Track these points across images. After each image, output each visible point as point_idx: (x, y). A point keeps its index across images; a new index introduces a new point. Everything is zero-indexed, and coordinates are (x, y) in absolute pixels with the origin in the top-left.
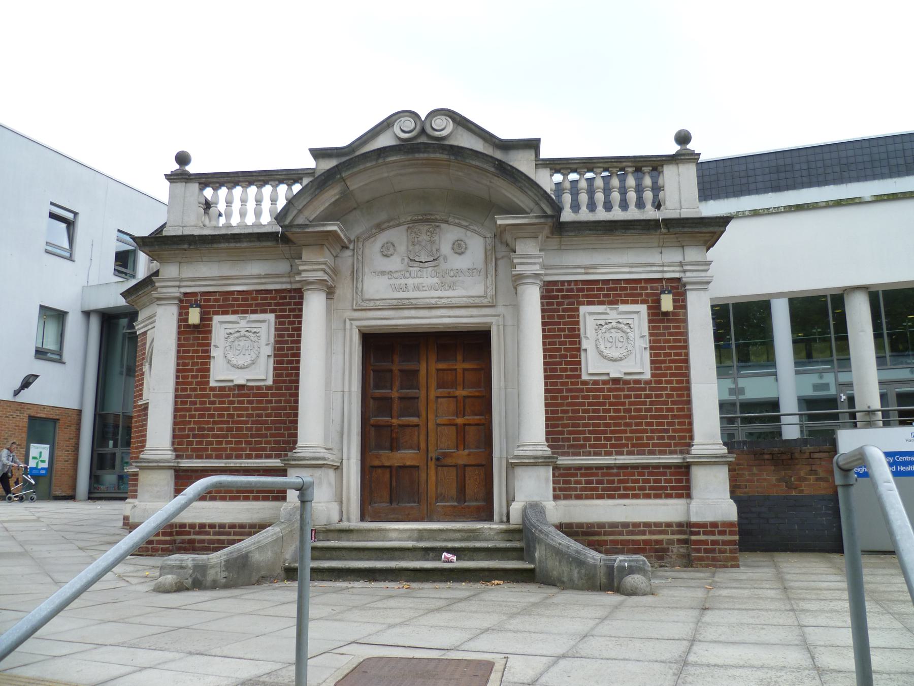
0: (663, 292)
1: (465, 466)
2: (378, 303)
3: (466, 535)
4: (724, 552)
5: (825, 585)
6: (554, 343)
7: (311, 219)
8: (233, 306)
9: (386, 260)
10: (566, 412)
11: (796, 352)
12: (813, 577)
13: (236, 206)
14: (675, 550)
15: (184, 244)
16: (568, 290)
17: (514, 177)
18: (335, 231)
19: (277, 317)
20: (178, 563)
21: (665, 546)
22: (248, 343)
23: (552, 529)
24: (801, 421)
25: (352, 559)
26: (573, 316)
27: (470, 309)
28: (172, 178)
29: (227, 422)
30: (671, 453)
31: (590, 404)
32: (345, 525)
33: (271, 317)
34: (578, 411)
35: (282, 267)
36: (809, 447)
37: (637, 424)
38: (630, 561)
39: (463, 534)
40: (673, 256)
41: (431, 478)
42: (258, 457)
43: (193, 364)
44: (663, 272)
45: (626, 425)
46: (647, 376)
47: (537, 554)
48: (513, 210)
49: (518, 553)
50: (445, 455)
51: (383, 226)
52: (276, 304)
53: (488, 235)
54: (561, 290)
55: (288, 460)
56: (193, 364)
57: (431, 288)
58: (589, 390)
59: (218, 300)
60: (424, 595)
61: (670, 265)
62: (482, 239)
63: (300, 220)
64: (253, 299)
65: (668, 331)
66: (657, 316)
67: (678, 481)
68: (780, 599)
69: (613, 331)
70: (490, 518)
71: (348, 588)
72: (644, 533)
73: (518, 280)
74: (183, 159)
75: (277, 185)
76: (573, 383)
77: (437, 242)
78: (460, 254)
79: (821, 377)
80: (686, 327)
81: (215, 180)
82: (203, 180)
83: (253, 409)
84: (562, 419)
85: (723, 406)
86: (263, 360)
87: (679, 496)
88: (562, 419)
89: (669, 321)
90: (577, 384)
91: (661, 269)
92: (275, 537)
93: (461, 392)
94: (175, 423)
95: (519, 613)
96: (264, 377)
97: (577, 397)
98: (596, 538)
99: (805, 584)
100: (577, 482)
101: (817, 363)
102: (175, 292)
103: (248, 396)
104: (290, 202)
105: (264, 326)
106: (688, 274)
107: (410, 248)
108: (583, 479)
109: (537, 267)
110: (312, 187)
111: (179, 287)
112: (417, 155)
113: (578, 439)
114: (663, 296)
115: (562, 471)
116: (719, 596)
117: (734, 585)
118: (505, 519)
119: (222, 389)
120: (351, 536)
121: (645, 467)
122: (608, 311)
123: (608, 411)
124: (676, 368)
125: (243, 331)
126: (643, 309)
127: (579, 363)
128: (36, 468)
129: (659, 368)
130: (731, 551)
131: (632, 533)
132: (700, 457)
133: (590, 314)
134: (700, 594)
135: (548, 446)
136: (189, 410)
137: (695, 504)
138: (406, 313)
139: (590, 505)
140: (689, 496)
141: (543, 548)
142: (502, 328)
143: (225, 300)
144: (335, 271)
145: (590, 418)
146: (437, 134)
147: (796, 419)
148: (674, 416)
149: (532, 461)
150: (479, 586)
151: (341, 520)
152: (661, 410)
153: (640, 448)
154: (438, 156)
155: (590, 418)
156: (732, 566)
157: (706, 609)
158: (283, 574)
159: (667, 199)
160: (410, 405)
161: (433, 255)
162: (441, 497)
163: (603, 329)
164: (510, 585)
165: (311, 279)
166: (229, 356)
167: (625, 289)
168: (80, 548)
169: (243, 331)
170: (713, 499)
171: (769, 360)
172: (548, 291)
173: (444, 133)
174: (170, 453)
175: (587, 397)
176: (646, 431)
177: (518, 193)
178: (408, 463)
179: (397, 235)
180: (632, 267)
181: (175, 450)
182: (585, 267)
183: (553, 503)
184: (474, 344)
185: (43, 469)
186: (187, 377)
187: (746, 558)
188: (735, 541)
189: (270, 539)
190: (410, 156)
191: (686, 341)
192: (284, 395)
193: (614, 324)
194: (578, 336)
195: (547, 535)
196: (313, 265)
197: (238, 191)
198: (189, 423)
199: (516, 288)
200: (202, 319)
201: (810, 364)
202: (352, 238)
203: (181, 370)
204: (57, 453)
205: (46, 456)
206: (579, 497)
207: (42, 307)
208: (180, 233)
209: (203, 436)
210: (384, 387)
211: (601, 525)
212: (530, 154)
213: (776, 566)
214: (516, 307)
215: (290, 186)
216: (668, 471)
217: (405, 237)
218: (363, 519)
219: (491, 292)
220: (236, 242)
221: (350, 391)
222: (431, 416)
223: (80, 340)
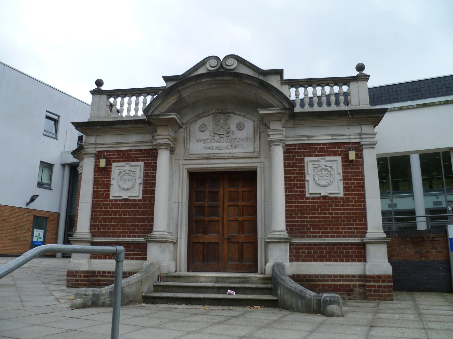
0: (350, 150)
1: (243, 243)
2: (197, 156)
3: (241, 280)
4: (385, 292)
5: (442, 312)
6: (291, 177)
7: (162, 112)
8: (122, 158)
10: (298, 214)
11: (424, 185)
12: (436, 307)
13: (126, 106)
14: (357, 290)
16: (298, 149)
18: (174, 118)
19: (145, 164)
20: (84, 292)
21: (352, 288)
22: (130, 177)
23: (288, 278)
24: (427, 220)
25: (179, 292)
26: (301, 163)
27: (244, 159)
28: (93, 92)
29: (118, 218)
30: (355, 237)
31: (310, 210)
32: (178, 273)
33: (142, 163)
34: (304, 214)
35: (148, 137)
36: (432, 235)
37: (336, 221)
38: (330, 297)
39: (240, 280)
40: (355, 130)
42: (134, 236)
44: (350, 139)
45: (330, 221)
46: (342, 195)
47: (279, 292)
48: (268, 106)
49: (270, 291)
50: (233, 237)
52: (145, 157)
53: (256, 120)
54: (295, 149)
55: (148, 238)
57: (226, 148)
58: (309, 202)
59: (115, 155)
60: (219, 314)
62: (252, 122)
63: (157, 113)
66: (347, 162)
67: (359, 253)
68: (417, 321)
69: (323, 170)
70: (256, 271)
71: (175, 308)
72: (340, 281)
73: (271, 143)
74: (99, 83)
75: (146, 96)
76: (301, 199)
77: (229, 124)
78: (241, 130)
79: (437, 198)
80: (363, 169)
81: (115, 93)
82: (109, 94)
83: (132, 211)
84: (295, 218)
85: (384, 213)
86: (137, 186)
87: (359, 261)
88: (295, 218)
89: (354, 165)
90: (303, 199)
91: (348, 137)
92: (137, 280)
93: (241, 203)
94: (92, 219)
95: (264, 327)
96: (137, 195)
98: (313, 283)
99: (431, 312)
100: (303, 252)
101: (435, 191)
102: (93, 151)
103: (129, 204)
105: (138, 168)
106: (364, 140)
107: (215, 127)
108: (306, 250)
109: (281, 136)
111: (95, 148)
112: (217, 78)
113: (304, 229)
114: (350, 152)
115: (295, 246)
116: (381, 318)
117: (391, 311)
118: (264, 272)
119: (116, 201)
122: (320, 160)
123: (320, 214)
124: (358, 191)
125: (127, 171)
126: (339, 158)
127: (304, 188)
128: (37, 242)
129: (348, 191)
130: (389, 292)
131: (333, 281)
132: (371, 239)
133: (311, 161)
134: (370, 316)
135: (288, 233)
136: (99, 212)
137: (368, 265)
138: (212, 161)
140: (365, 261)
141: (282, 289)
142: (263, 169)
144: (175, 140)
145: (310, 218)
146: (229, 67)
147: (424, 219)
148: (357, 217)
149: (278, 240)
150: (246, 309)
151: (176, 271)
152: (349, 213)
153: (338, 234)
154: (228, 78)
155: (310, 218)
156: (389, 300)
157: (372, 326)
158: (142, 300)
159: (352, 100)
160: (214, 210)
161: (226, 131)
163: (318, 170)
164: (264, 309)
165: (161, 143)
166: (120, 184)
167: (329, 148)
168: (43, 283)
169: (127, 171)
170: (378, 262)
171: (410, 189)
172: (287, 149)
173: (232, 67)
174: (88, 234)
175: (309, 206)
176: (341, 225)
178: (213, 241)
179: (208, 121)
180: (333, 136)
181: (91, 232)
183: (289, 264)
184: (248, 178)
185: (40, 242)
186: (98, 194)
187: (396, 295)
188: (391, 286)
189: (135, 281)
190: (214, 79)
191: (363, 176)
192: (148, 204)
193: (323, 167)
194: (304, 173)
195: (284, 281)
196: (163, 136)
197: (126, 99)
198: (99, 218)
199: (270, 148)
200: (106, 165)
201: (431, 191)
202: (184, 123)
203: (96, 191)
204: (47, 234)
205: (42, 235)
206: (304, 260)
207: (41, 162)
208: (96, 120)
209: (106, 225)
211: (316, 276)
212: (278, 78)
213: (414, 300)
214: (270, 157)
215: (153, 96)
216: (353, 246)
218: (188, 270)
219: (257, 150)
220: (124, 125)
221: (182, 202)
222: (225, 216)
223: (59, 178)
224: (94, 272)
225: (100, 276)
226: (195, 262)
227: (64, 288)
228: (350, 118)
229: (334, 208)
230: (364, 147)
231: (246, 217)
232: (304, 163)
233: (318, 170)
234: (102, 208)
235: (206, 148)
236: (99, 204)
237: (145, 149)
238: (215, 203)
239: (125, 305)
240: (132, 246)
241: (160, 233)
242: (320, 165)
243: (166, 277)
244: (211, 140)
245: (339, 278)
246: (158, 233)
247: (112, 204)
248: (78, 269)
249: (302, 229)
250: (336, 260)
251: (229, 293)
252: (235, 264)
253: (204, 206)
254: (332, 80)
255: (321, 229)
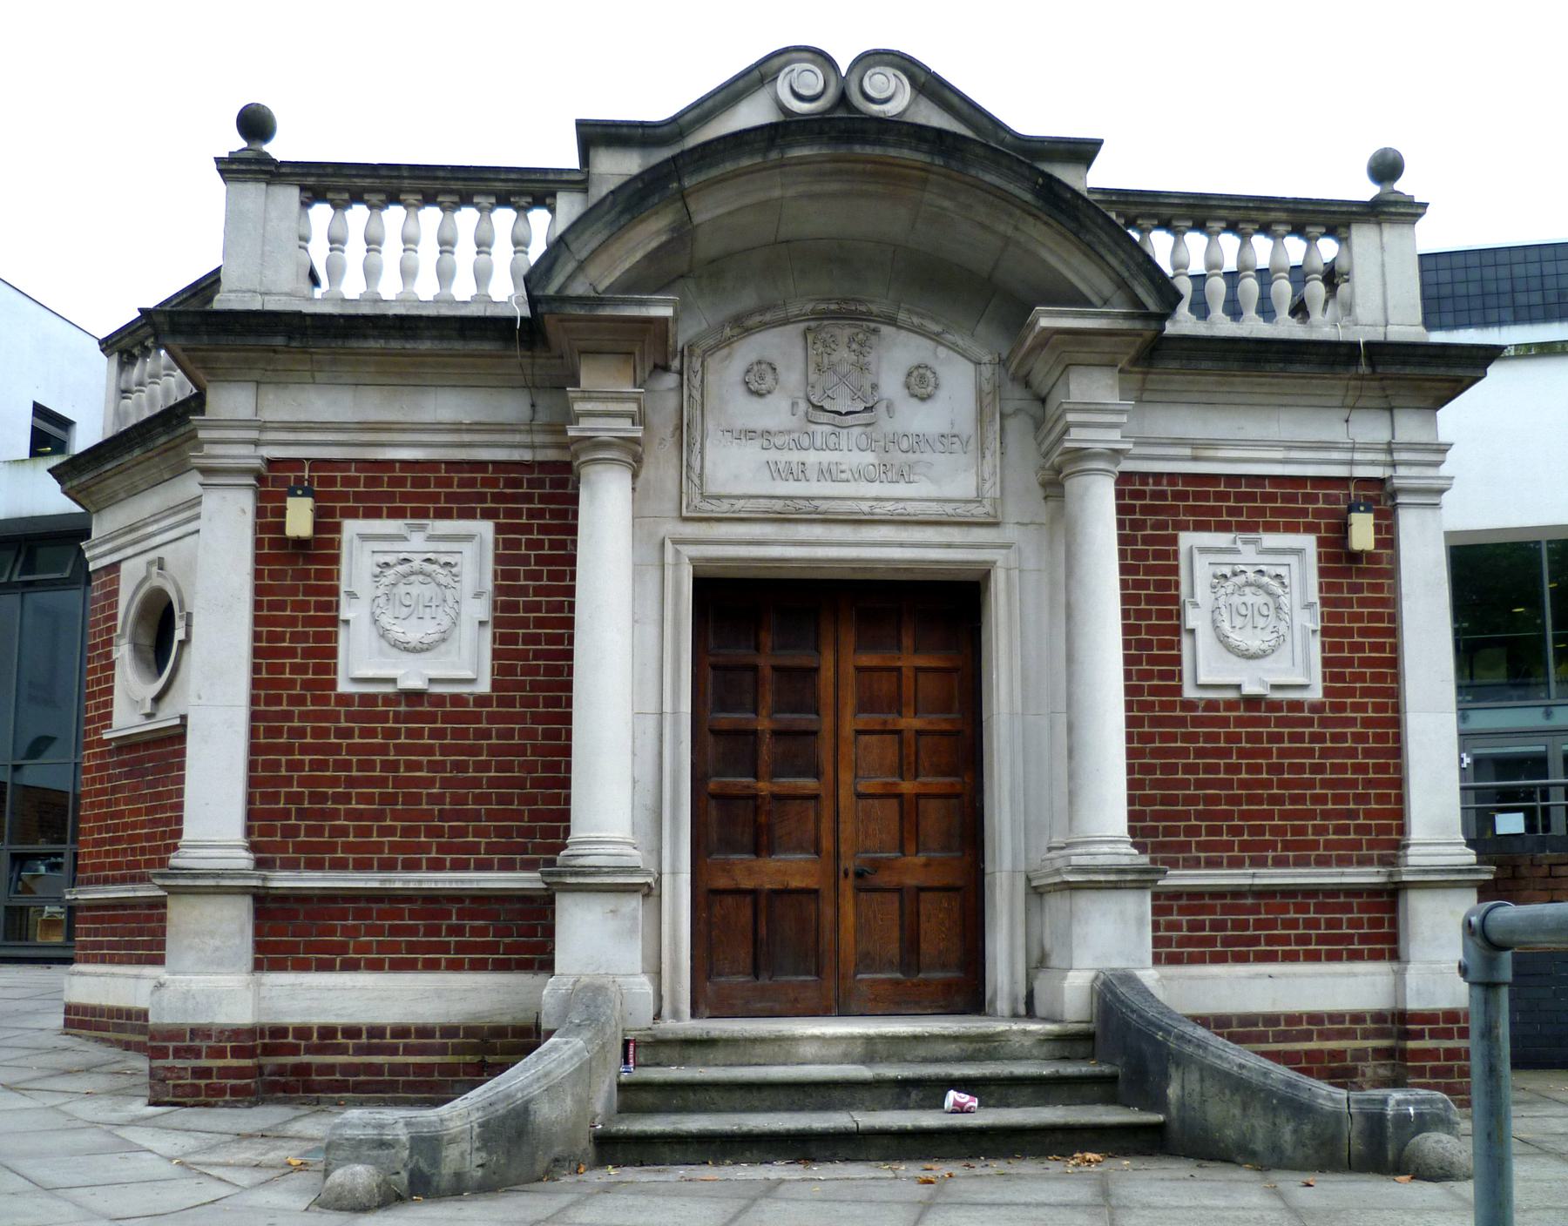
0: (1350, 510)
1: (920, 889)
2: (740, 504)
3: (970, 1047)
7: (601, 288)
8: (390, 497)
9: (756, 403)
13: (355, 251)
14: (1369, 1072)
15: (275, 334)
17: (1076, 219)
19: (499, 529)
20: (371, 1133)
21: (1349, 1063)
22: (429, 591)
27: (945, 529)
28: (231, 168)
29: (382, 782)
30: (1362, 862)
31: (1200, 753)
33: (484, 529)
34: (1173, 769)
35: (510, 407)
37: (1295, 799)
38: (1417, 1103)
39: (964, 1045)
40: (1370, 429)
41: (849, 920)
43: (295, 637)
44: (1351, 463)
46: (1316, 694)
47: (1173, 1091)
48: (1073, 298)
50: (877, 865)
51: (750, 322)
52: (497, 498)
55: (559, 874)
56: (295, 637)
57: (860, 475)
58: (1198, 722)
59: (353, 482)
61: (1367, 448)
62: (971, 366)
63: (579, 288)
64: (441, 482)
65: (1358, 591)
66: (1339, 560)
67: (1376, 925)
69: (1247, 590)
72: (1307, 1036)
74: (255, 124)
76: (1165, 706)
77: (873, 367)
79: (1548, 715)
80: (1396, 588)
81: (342, 182)
82: (311, 181)
83: (445, 750)
87: (1376, 956)
89: (1362, 573)
90: (1170, 706)
92: (576, 1062)
93: (910, 722)
96: (469, 674)
97: (1173, 737)
102: (251, 457)
103: (432, 718)
104: (558, 247)
106: (1401, 471)
107: (813, 377)
108: (1185, 918)
109: (1115, 435)
110: (613, 205)
111: (256, 443)
112: (858, 149)
118: (1022, 1009)
120: (711, 1054)
121: (1310, 892)
122: (1239, 545)
126: (1308, 542)
127: (1177, 660)
132: (1426, 872)
133: (1205, 550)
135: (1134, 845)
136: (288, 749)
138: (803, 532)
139: (1203, 978)
140: (1394, 956)
141: (1195, 1076)
143: (371, 482)
145: (1200, 784)
146: (875, 109)
148: (1369, 783)
149: (1113, 878)
151: (658, 1016)
153: (1300, 851)
154: (906, 153)
155: (1200, 784)
160: (798, 749)
162: (867, 961)
163: (1229, 585)
165: (604, 436)
166: (386, 620)
174: (245, 854)
175: (1193, 738)
176: (1311, 815)
177: (1077, 259)
178: (795, 883)
179: (778, 344)
180: (1290, 448)
181: (253, 847)
182: (1193, 444)
184: (945, 611)
189: (568, 1068)
190: (843, 150)
191: (1394, 618)
192: (520, 718)
193: (1251, 576)
194: (1176, 599)
196: (604, 399)
200: (318, 527)
203: (265, 652)
208: (256, 305)
210: (738, 707)
216: (1355, 901)
217: (798, 352)
219: (991, 491)
220: (407, 338)
222: (846, 777)
224: (279, 1031)
225: (309, 1051)
226: (720, 975)
227: (140, 1108)
228: (1362, 378)
229: (1286, 745)
230: (1401, 499)
231: (933, 782)
232: (1176, 557)
233: (1229, 591)
234: (301, 733)
235: (778, 472)
236: (288, 716)
237: (495, 463)
238: (802, 720)
239: (540, 1180)
240: (454, 908)
241: (610, 849)
242: (1238, 568)
243: (648, 1045)
244: (796, 436)
245: (1305, 1027)
246: (602, 849)
247: (351, 717)
248: (202, 1020)
249: (1168, 831)
250: (1291, 957)
251: (956, 1103)
252: (890, 980)
253: (755, 732)
254: (1286, 210)
255: (1236, 831)
